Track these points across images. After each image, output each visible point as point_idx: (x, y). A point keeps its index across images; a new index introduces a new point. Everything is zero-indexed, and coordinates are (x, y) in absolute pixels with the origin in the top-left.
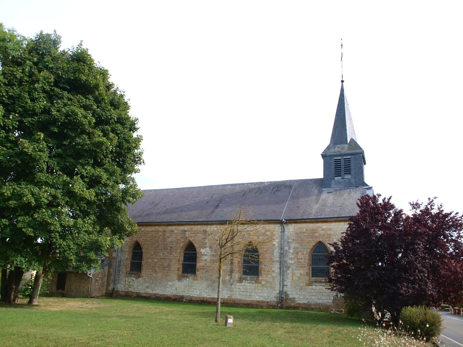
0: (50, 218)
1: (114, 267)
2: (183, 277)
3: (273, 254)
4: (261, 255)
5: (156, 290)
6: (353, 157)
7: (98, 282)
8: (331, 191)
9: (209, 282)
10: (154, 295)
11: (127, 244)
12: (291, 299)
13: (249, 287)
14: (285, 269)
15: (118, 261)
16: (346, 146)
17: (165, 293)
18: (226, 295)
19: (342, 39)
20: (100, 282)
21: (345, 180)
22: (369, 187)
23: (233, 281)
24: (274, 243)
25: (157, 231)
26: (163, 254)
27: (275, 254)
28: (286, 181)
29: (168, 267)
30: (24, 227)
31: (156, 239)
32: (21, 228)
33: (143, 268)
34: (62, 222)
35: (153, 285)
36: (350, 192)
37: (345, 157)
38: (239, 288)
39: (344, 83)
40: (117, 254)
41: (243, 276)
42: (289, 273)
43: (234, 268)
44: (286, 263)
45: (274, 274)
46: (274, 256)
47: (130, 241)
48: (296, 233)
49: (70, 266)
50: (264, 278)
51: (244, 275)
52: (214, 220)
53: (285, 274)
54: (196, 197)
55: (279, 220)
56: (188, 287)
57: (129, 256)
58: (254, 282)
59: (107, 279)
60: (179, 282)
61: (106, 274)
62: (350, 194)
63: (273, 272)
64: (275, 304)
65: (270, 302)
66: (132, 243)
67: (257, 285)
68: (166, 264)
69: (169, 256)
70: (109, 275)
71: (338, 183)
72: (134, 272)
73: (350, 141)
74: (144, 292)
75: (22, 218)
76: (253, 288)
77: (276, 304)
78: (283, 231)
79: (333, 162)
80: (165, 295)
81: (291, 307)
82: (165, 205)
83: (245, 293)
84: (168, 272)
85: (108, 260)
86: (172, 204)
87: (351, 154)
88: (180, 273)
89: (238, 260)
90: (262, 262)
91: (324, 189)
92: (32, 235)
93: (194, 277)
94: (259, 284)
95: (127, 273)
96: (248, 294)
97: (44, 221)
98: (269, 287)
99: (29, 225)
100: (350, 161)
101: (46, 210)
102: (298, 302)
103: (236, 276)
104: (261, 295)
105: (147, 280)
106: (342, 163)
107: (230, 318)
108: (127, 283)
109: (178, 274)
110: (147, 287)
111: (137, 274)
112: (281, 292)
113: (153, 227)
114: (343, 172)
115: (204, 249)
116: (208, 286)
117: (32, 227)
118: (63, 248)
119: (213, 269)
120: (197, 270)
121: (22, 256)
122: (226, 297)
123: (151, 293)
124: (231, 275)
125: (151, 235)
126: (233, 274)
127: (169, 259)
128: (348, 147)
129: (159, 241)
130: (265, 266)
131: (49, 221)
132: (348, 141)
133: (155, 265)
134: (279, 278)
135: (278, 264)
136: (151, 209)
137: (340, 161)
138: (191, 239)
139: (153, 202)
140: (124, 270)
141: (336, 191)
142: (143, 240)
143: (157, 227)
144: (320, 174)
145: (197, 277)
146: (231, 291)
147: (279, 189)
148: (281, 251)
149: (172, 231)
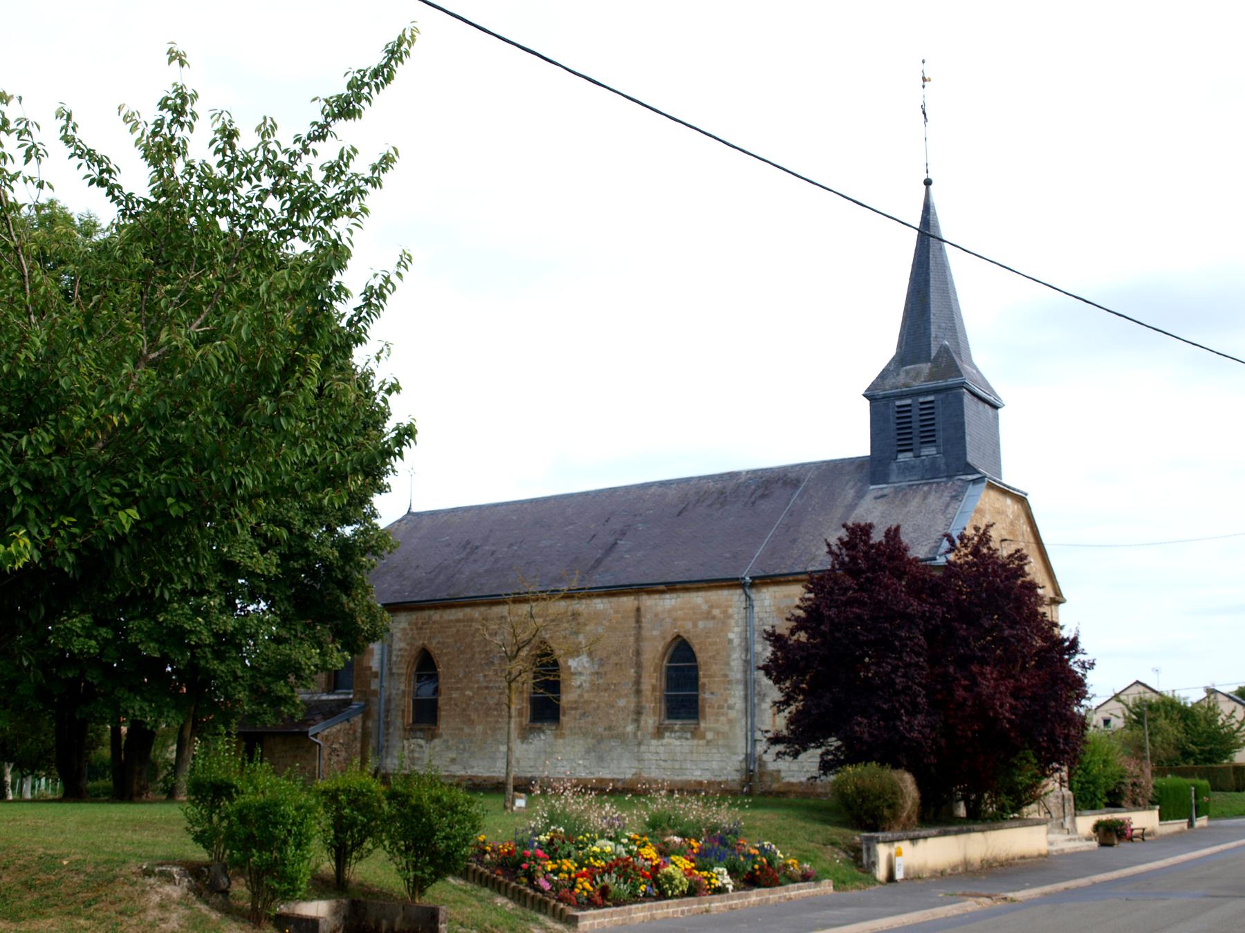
0: (189, 619)
1: (376, 717)
2: (532, 730)
3: (728, 664)
4: (703, 668)
5: (473, 767)
6: (941, 396)
7: (338, 755)
8: (886, 491)
9: (590, 741)
10: (469, 779)
11: (402, 656)
12: (771, 774)
13: (678, 749)
14: (756, 701)
15: (383, 702)
16: (925, 367)
17: (494, 774)
18: (628, 771)
19: (923, 62)
20: (343, 754)
21: (923, 461)
22: (979, 476)
23: (643, 735)
24: (731, 636)
25: (468, 621)
26: (485, 676)
27: (732, 664)
28: (793, 467)
29: (496, 709)
30: (141, 642)
31: (467, 640)
32: (137, 644)
33: (443, 713)
34: (214, 626)
35: (466, 755)
36: (929, 492)
37: (921, 400)
38: (657, 753)
39: (931, 187)
40: (381, 682)
41: (667, 722)
42: (765, 710)
43: (644, 704)
44: (759, 685)
45: (732, 714)
46: (731, 670)
47: (408, 648)
48: (779, 609)
49: (238, 712)
50: (711, 725)
51: (669, 718)
52: (594, 586)
53: (757, 711)
54: (570, 524)
55: (738, 579)
56: (543, 757)
57: (409, 684)
58: (689, 735)
59: (362, 747)
60: (523, 743)
61: (358, 735)
62: (925, 498)
63: (730, 707)
64: (737, 787)
65: (726, 782)
66: (413, 652)
67: (695, 742)
68: (492, 702)
69: (497, 681)
70: (365, 736)
71: (907, 469)
72: (422, 726)
73: (939, 352)
74: (447, 773)
75: (136, 623)
76: (686, 749)
77: (739, 788)
78: (749, 606)
79: (892, 413)
80: (493, 777)
81: (771, 793)
82: (493, 548)
83: (670, 762)
84: (497, 722)
85: (360, 700)
86: (511, 545)
87: (935, 391)
88: (526, 720)
89: (652, 680)
90: (704, 684)
91: (872, 487)
92: (157, 655)
93: (556, 729)
94: (700, 739)
95: (405, 730)
96: (677, 766)
97: (176, 626)
98: (722, 746)
99: (149, 636)
100: (932, 408)
101: (179, 604)
102: (787, 780)
103: (650, 721)
104: (706, 766)
105: (451, 743)
106: (915, 411)
107: (521, 798)
108: (406, 753)
109: (521, 723)
110: (453, 761)
111: (429, 729)
112: (749, 758)
113: (459, 610)
114: (916, 440)
115: (577, 660)
116: (588, 751)
117: (157, 641)
118: (222, 677)
119: (598, 708)
120: (561, 712)
121: (144, 699)
122: (629, 776)
123: (462, 776)
124: (637, 721)
125: (454, 630)
126: (643, 718)
127: (499, 688)
128: (931, 369)
129: (475, 644)
130: (712, 693)
131: (186, 626)
132: (933, 354)
133: (468, 705)
134: (743, 722)
135: (741, 687)
136: (460, 561)
137: (909, 411)
138: (547, 636)
139: (468, 542)
140: (399, 722)
141: (897, 491)
142: (438, 643)
143: (468, 610)
144: (859, 445)
145: (562, 729)
146: (639, 761)
147: (767, 492)
148: (746, 655)
149: (502, 617)
